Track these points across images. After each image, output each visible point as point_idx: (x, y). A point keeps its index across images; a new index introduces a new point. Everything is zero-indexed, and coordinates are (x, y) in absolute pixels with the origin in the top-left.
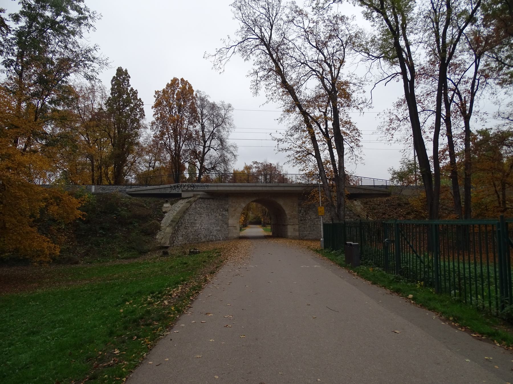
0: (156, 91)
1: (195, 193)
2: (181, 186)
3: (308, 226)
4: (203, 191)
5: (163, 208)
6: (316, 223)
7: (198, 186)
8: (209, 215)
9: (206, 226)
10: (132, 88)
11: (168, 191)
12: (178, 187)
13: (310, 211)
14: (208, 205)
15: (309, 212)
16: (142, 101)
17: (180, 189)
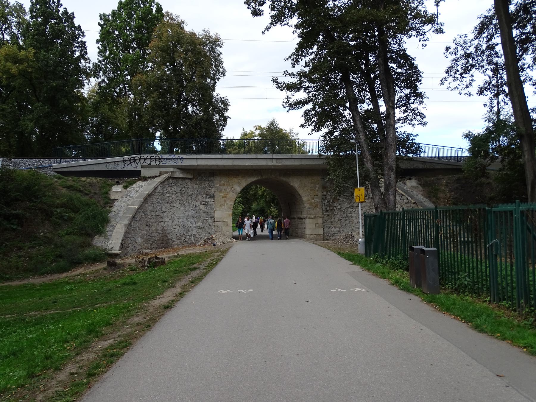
1: (163, 170)
2: (140, 159)
3: (336, 219)
4: (174, 167)
6: (349, 215)
7: (166, 159)
8: (184, 204)
9: (180, 220)
11: (119, 168)
12: (135, 160)
14: (184, 189)
17: (139, 164)
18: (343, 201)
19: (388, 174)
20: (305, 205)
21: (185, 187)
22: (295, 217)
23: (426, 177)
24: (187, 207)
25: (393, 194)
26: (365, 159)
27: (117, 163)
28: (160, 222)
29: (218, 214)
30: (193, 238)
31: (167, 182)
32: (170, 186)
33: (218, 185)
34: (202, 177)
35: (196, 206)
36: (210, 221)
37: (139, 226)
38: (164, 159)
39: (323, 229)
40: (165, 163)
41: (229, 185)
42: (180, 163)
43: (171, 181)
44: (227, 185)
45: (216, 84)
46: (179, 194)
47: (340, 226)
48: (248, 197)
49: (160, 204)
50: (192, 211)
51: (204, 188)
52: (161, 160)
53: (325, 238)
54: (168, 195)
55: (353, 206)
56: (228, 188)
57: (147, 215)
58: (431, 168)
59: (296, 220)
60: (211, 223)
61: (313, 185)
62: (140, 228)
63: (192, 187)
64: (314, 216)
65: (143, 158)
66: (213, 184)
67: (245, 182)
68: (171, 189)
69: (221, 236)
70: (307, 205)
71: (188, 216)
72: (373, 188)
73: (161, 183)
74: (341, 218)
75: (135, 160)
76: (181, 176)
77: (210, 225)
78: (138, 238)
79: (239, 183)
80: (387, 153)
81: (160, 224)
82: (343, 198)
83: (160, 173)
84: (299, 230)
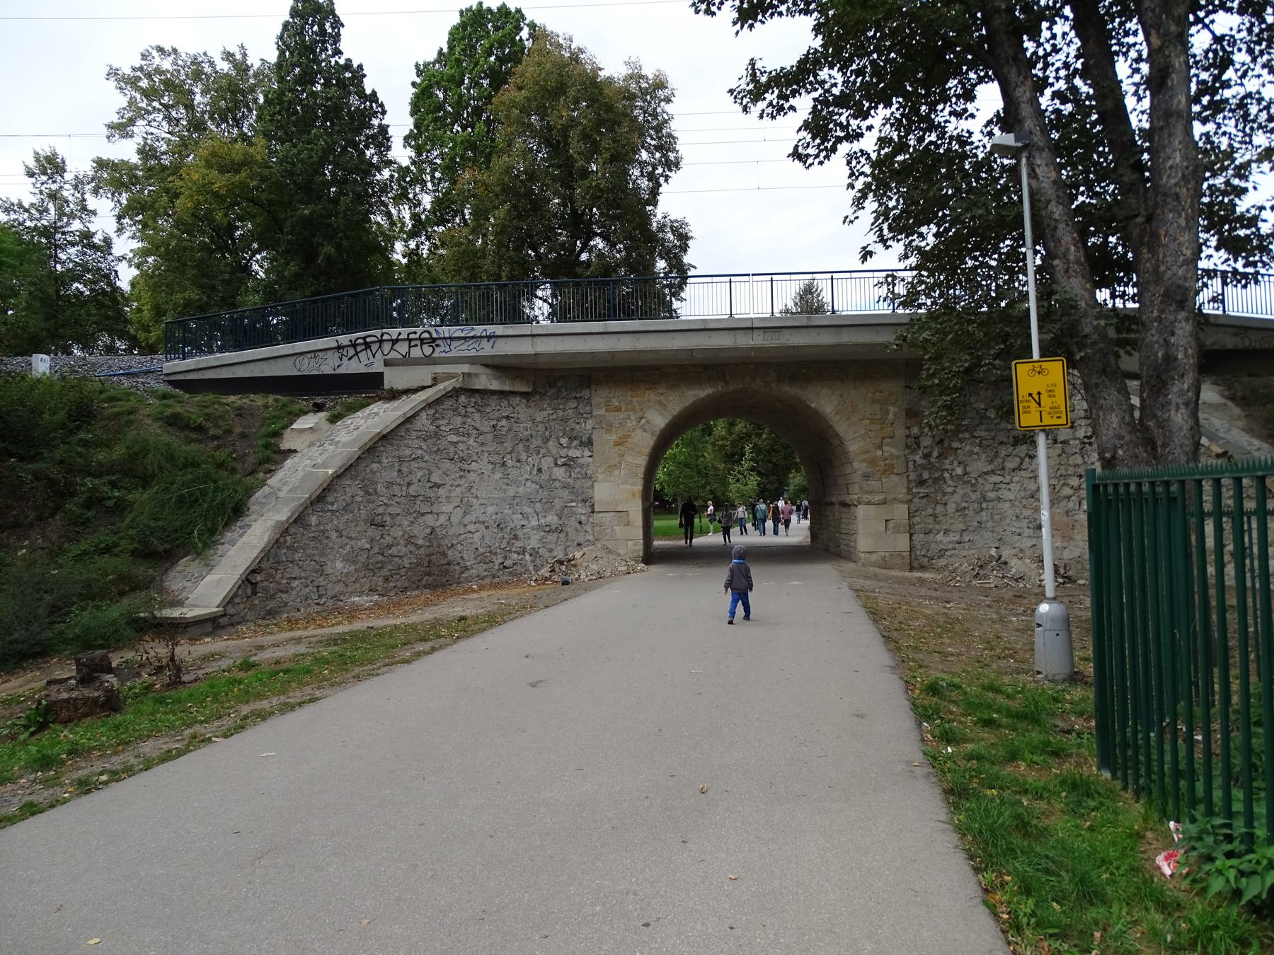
0: (417, 66)
1: (440, 369)
2: (381, 341)
3: (951, 507)
4: (473, 361)
5: (287, 433)
6: (992, 495)
7: (451, 338)
8: (504, 464)
9: (491, 510)
10: (349, 60)
11: (328, 366)
12: (367, 346)
13: (961, 441)
14: (504, 422)
15: (955, 445)
16: (381, 98)
17: (379, 355)
18: (971, 453)
19: (1159, 319)
20: (856, 465)
21: (508, 418)
22: (834, 500)
23: (1249, 375)
24: (513, 473)
25: (1187, 404)
26: (1056, 262)
27: (321, 354)
28: (422, 515)
29: (603, 492)
30: (528, 557)
31: (449, 403)
32: (459, 414)
33: (602, 412)
34: (559, 390)
35: (540, 470)
36: (580, 510)
37: (341, 527)
38: (445, 338)
39: (911, 535)
40: (447, 349)
41: (634, 410)
42: (487, 349)
43: (463, 399)
44: (627, 410)
45: (661, 189)
46: (490, 436)
47: (962, 526)
48: (774, 460)
49: (423, 465)
50: (529, 484)
51: (565, 420)
52: (437, 342)
53: (915, 564)
54: (454, 438)
55: (1003, 469)
56: (629, 418)
57: (376, 493)
58: (1267, 346)
59: (836, 507)
60: (583, 518)
61: (877, 407)
62: (344, 533)
63: (529, 418)
64: (882, 497)
65: (388, 337)
66: (588, 408)
67: (679, 401)
68: (464, 423)
69: (599, 554)
70: (860, 466)
71: (514, 497)
72: (1095, 379)
73: (430, 405)
74: (966, 505)
75: (367, 346)
76: (495, 385)
77: (580, 523)
78: (333, 561)
79: (660, 403)
80: (1155, 235)
81: (421, 520)
82: (971, 444)
83: (435, 379)
84: (843, 536)
